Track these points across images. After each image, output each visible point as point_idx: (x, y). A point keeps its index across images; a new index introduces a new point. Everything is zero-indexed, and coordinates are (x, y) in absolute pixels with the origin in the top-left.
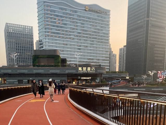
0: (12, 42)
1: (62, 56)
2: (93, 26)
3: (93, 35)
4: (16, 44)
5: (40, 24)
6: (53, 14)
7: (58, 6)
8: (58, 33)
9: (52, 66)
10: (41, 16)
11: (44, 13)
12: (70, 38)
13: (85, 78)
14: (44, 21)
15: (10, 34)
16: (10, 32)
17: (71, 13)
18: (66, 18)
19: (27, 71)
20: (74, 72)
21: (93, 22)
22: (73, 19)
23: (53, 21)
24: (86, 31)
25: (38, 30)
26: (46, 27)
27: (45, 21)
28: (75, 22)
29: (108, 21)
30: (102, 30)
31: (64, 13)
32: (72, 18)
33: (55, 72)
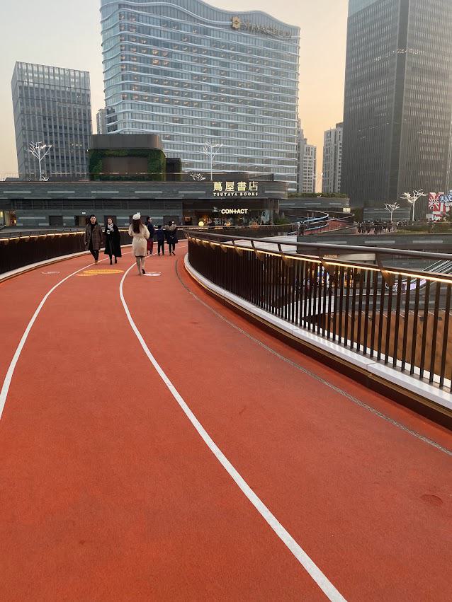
0: (33, 113)
1: (168, 152)
2: (253, 69)
3: (252, 95)
4: (44, 119)
5: (110, 64)
8: (157, 90)
9: (142, 178)
10: (112, 44)
11: (121, 35)
12: (191, 103)
13: (231, 211)
15: (26, 93)
16: (26, 88)
17: (193, 34)
18: (180, 47)
20: (200, 193)
21: (253, 60)
22: (200, 50)
23: (144, 58)
24: (234, 83)
25: (105, 81)
26: (125, 72)
27: (122, 56)
29: (295, 58)
30: (277, 81)
31: (173, 36)
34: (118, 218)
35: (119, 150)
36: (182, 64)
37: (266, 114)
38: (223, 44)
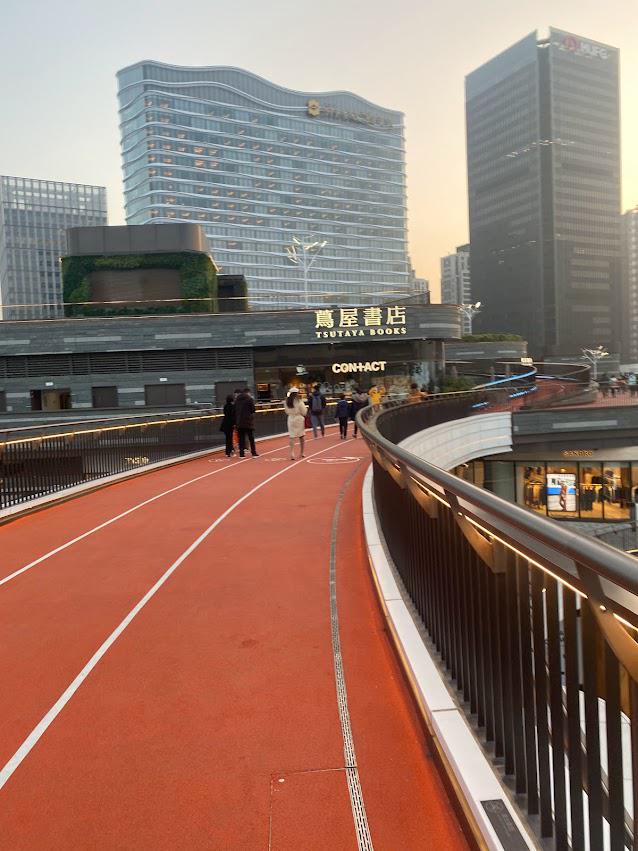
0: (25, 246)
1: (222, 264)
2: (340, 170)
3: (341, 206)
4: (41, 253)
5: (132, 169)
6: (181, 132)
7: (202, 102)
8: (203, 203)
9: (171, 309)
10: (135, 140)
11: (148, 128)
12: (253, 220)
13: (351, 367)
14: (147, 159)
15: (15, 218)
16: (14, 211)
17: (253, 124)
18: (234, 142)
19: (28, 342)
20: (289, 334)
21: (340, 158)
22: (263, 146)
23: (183, 158)
24: (314, 191)
25: (125, 193)
26: (154, 179)
27: (150, 156)
28: (271, 157)
29: (399, 154)
30: (376, 187)
31: (223, 127)
32: (256, 143)
33: (183, 340)
34: (120, 391)
35: (122, 257)
36: (238, 165)
37: (362, 233)
38: (296, 137)
